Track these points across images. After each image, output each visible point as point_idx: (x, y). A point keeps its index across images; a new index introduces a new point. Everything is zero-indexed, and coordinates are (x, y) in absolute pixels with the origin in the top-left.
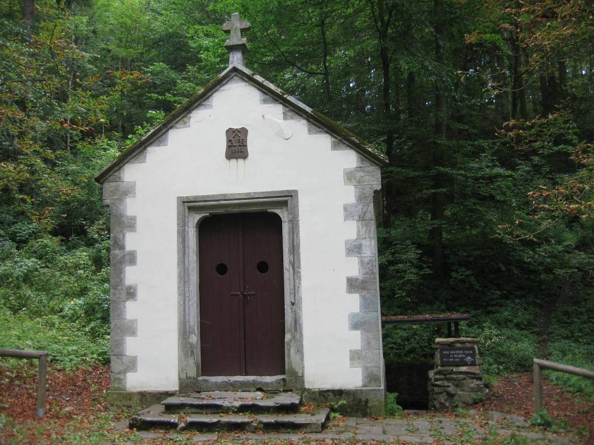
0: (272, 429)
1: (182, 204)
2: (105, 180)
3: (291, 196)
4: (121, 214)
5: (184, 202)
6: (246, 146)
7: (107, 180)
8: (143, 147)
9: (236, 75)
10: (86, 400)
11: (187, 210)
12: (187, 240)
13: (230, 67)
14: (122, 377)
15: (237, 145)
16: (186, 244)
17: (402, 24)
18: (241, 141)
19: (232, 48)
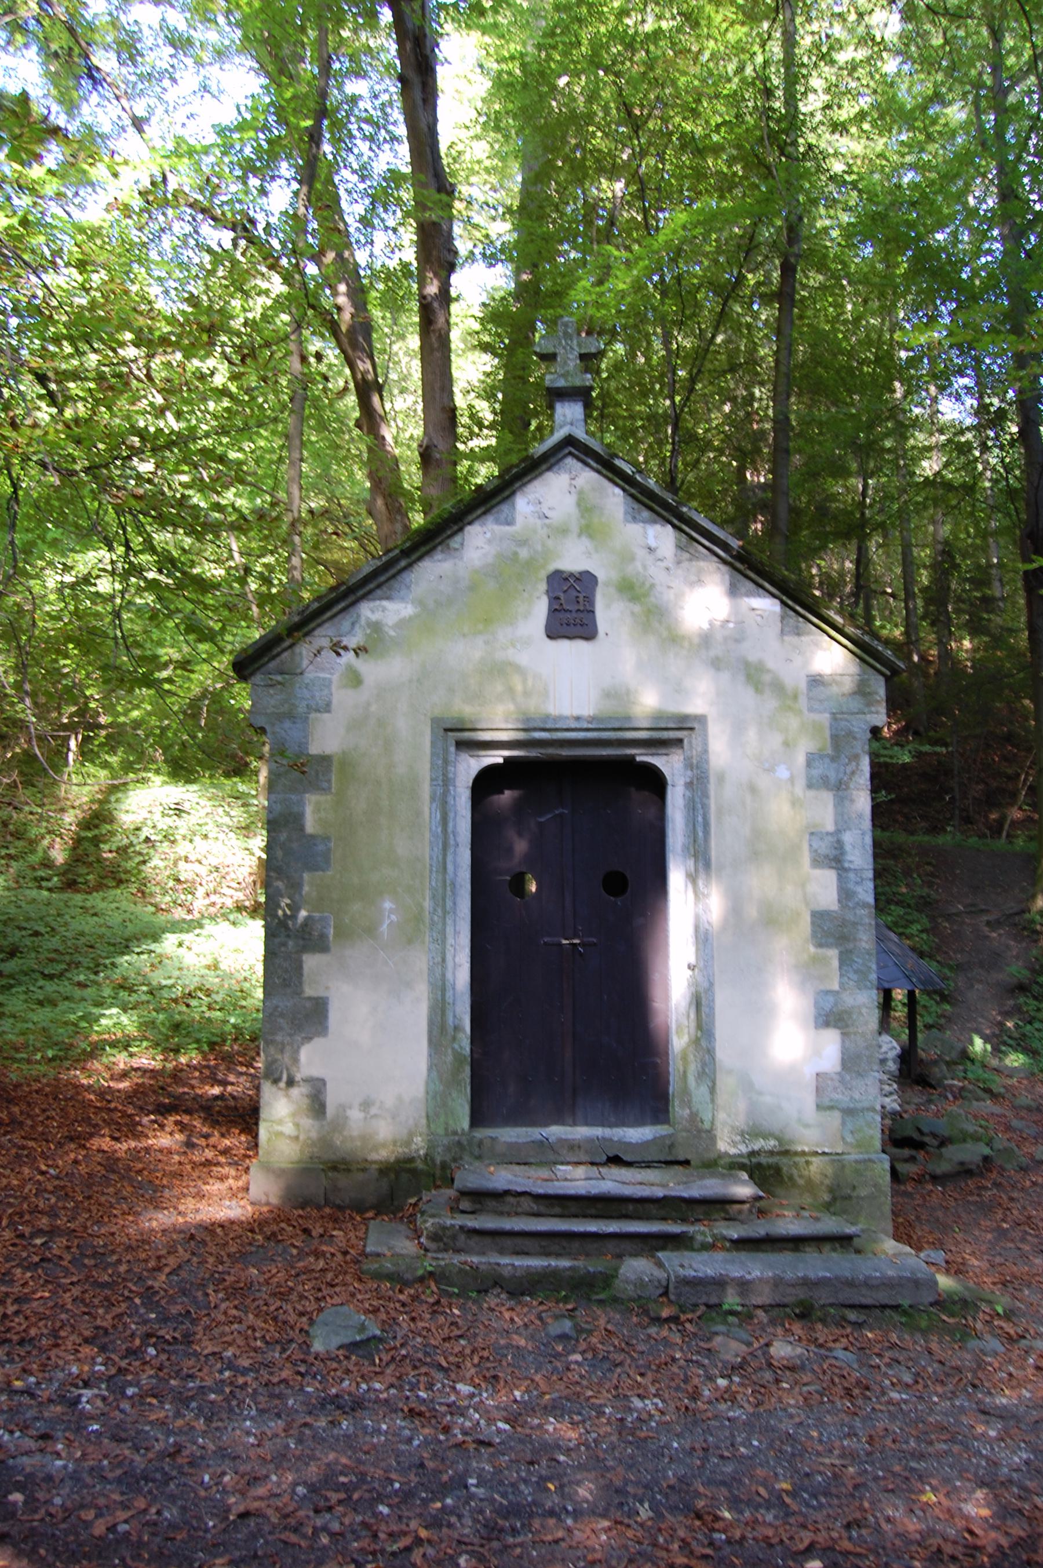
0: (429, 531)
1: (442, 732)
2: (258, 669)
3: (692, 729)
4: (434, 1098)
5: (447, 730)
6: (593, 612)
7: (263, 670)
8: (351, 598)
9: (570, 454)
10: (384, 1509)
11: (453, 749)
12: (451, 815)
13: (559, 435)
14: (107, 687)
15: (573, 607)
16: (451, 825)
17: (940, 226)
18: (581, 599)
19: (557, 395)
